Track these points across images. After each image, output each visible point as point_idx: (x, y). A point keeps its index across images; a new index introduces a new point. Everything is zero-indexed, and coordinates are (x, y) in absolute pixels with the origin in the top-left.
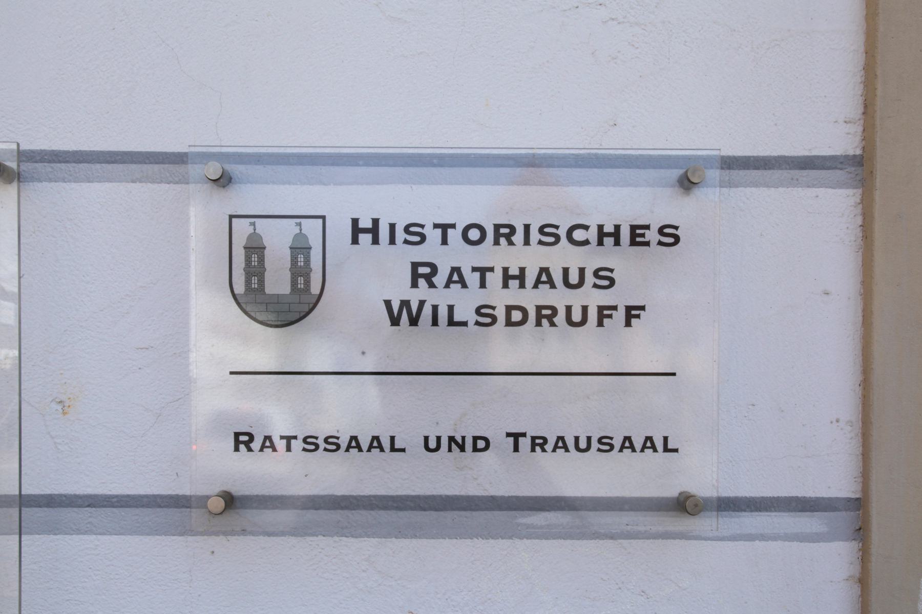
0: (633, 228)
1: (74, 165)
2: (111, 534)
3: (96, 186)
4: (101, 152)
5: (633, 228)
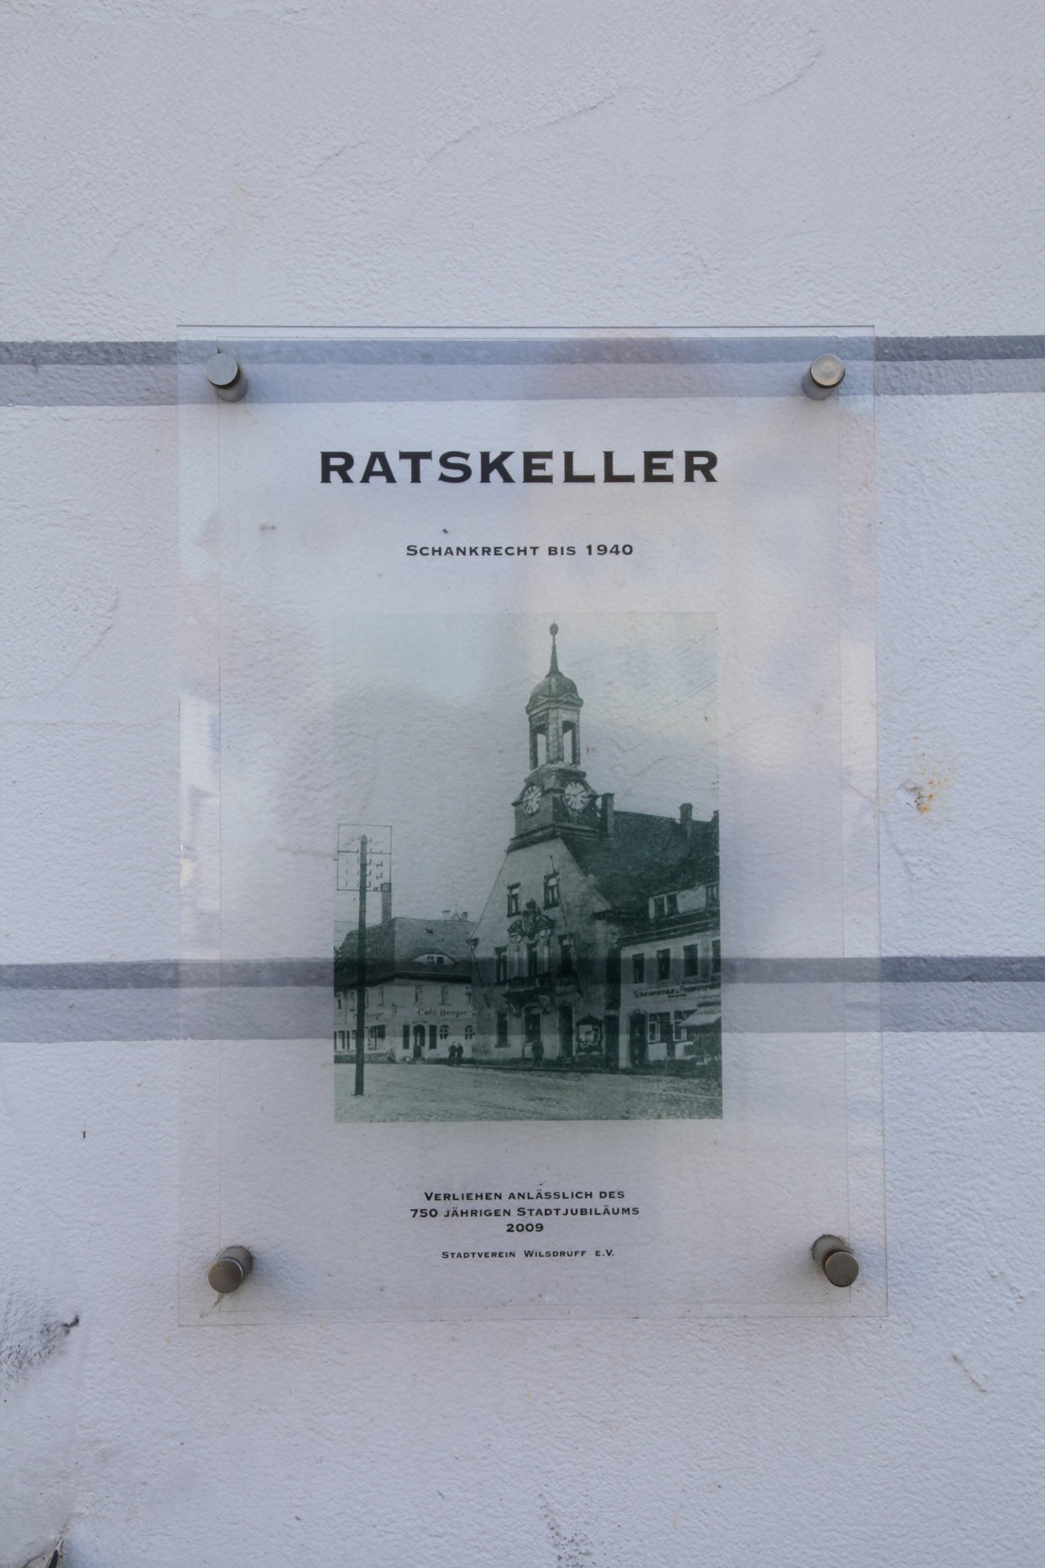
0: (528, 456)
1: (936, 362)
2: (1010, 1030)
3: (978, 400)
4: (986, 337)
5: (528, 456)
